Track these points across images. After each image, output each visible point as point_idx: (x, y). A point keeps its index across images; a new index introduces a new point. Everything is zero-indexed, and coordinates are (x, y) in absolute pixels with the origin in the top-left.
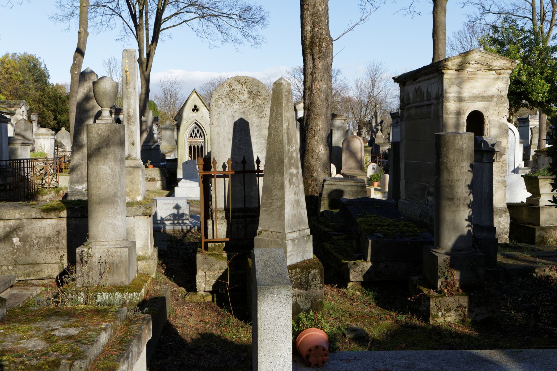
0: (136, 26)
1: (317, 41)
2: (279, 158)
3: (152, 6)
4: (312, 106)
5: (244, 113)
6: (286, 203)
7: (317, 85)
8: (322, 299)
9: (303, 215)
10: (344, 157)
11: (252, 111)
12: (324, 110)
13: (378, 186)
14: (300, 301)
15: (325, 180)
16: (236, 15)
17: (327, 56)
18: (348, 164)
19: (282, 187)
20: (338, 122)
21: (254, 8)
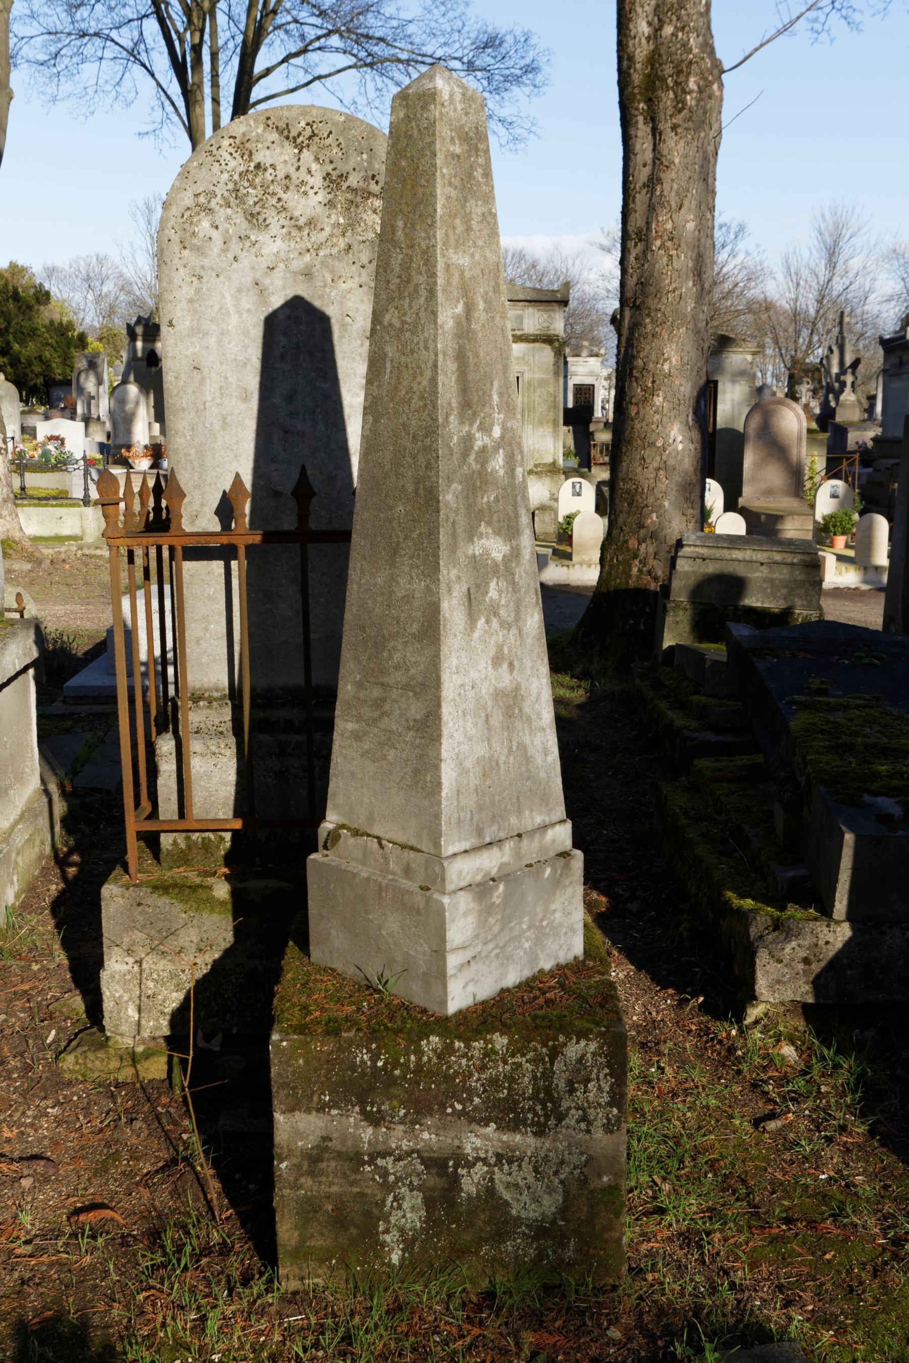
0: (187, 93)
1: (668, 70)
2: (418, 481)
3: (228, 30)
4: (645, 295)
5: (307, 274)
6: (446, 710)
7: (664, 222)
8: (617, 1175)
9: (539, 759)
10: (749, 459)
11: (344, 267)
12: (689, 306)
13: (847, 546)
14: (508, 1186)
15: (679, 544)
16: (460, 59)
17: (703, 121)
18: (760, 478)
19: (430, 630)
20: (737, 358)
21: (509, 39)
